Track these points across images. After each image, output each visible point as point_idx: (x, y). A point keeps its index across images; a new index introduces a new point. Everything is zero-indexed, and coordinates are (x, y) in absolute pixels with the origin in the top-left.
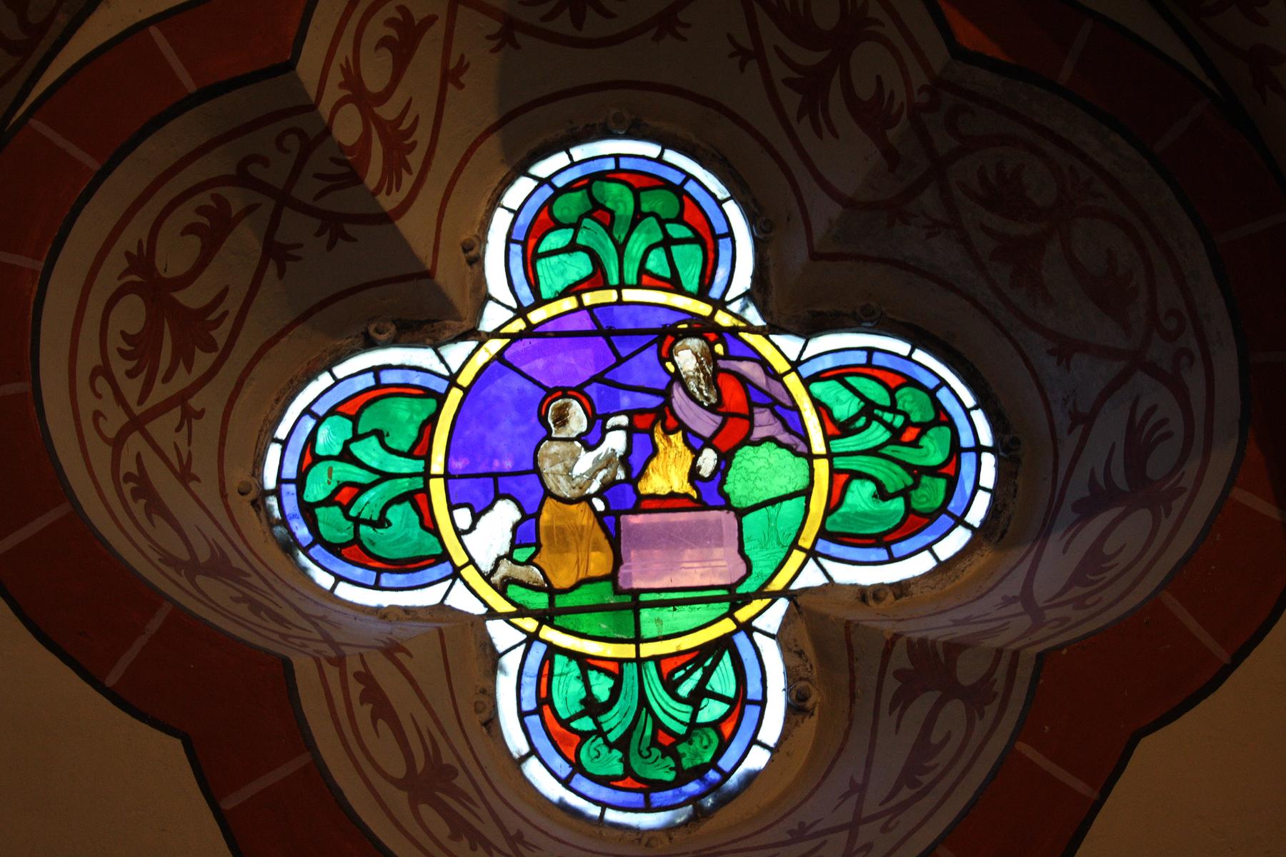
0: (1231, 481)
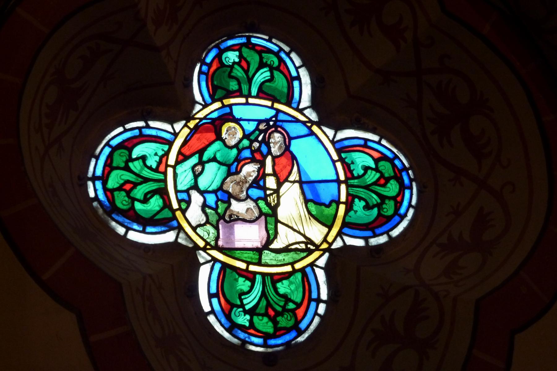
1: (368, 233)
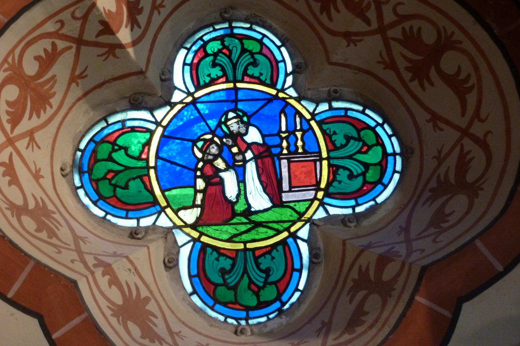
0: (479, 236)
1: (352, 202)
